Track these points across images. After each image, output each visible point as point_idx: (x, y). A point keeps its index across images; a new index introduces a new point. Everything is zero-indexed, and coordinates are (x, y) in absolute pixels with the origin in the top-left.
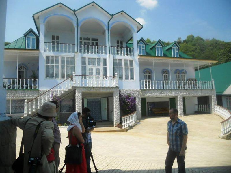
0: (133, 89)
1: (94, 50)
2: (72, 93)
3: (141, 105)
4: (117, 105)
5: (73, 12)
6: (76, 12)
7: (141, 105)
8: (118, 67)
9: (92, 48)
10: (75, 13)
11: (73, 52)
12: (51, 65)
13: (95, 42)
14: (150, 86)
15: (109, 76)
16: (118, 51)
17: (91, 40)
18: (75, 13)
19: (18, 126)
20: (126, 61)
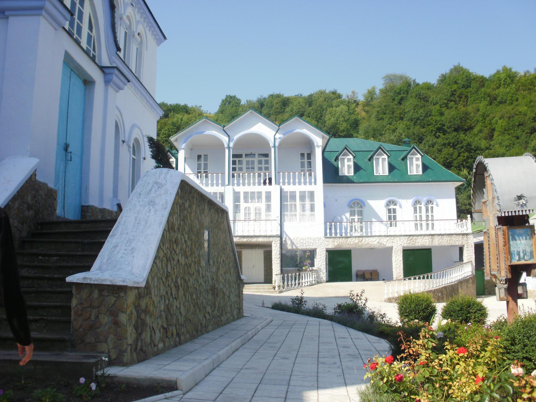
6: (225, 128)
8: (289, 203)
11: (223, 184)
14: (338, 231)
18: (224, 130)
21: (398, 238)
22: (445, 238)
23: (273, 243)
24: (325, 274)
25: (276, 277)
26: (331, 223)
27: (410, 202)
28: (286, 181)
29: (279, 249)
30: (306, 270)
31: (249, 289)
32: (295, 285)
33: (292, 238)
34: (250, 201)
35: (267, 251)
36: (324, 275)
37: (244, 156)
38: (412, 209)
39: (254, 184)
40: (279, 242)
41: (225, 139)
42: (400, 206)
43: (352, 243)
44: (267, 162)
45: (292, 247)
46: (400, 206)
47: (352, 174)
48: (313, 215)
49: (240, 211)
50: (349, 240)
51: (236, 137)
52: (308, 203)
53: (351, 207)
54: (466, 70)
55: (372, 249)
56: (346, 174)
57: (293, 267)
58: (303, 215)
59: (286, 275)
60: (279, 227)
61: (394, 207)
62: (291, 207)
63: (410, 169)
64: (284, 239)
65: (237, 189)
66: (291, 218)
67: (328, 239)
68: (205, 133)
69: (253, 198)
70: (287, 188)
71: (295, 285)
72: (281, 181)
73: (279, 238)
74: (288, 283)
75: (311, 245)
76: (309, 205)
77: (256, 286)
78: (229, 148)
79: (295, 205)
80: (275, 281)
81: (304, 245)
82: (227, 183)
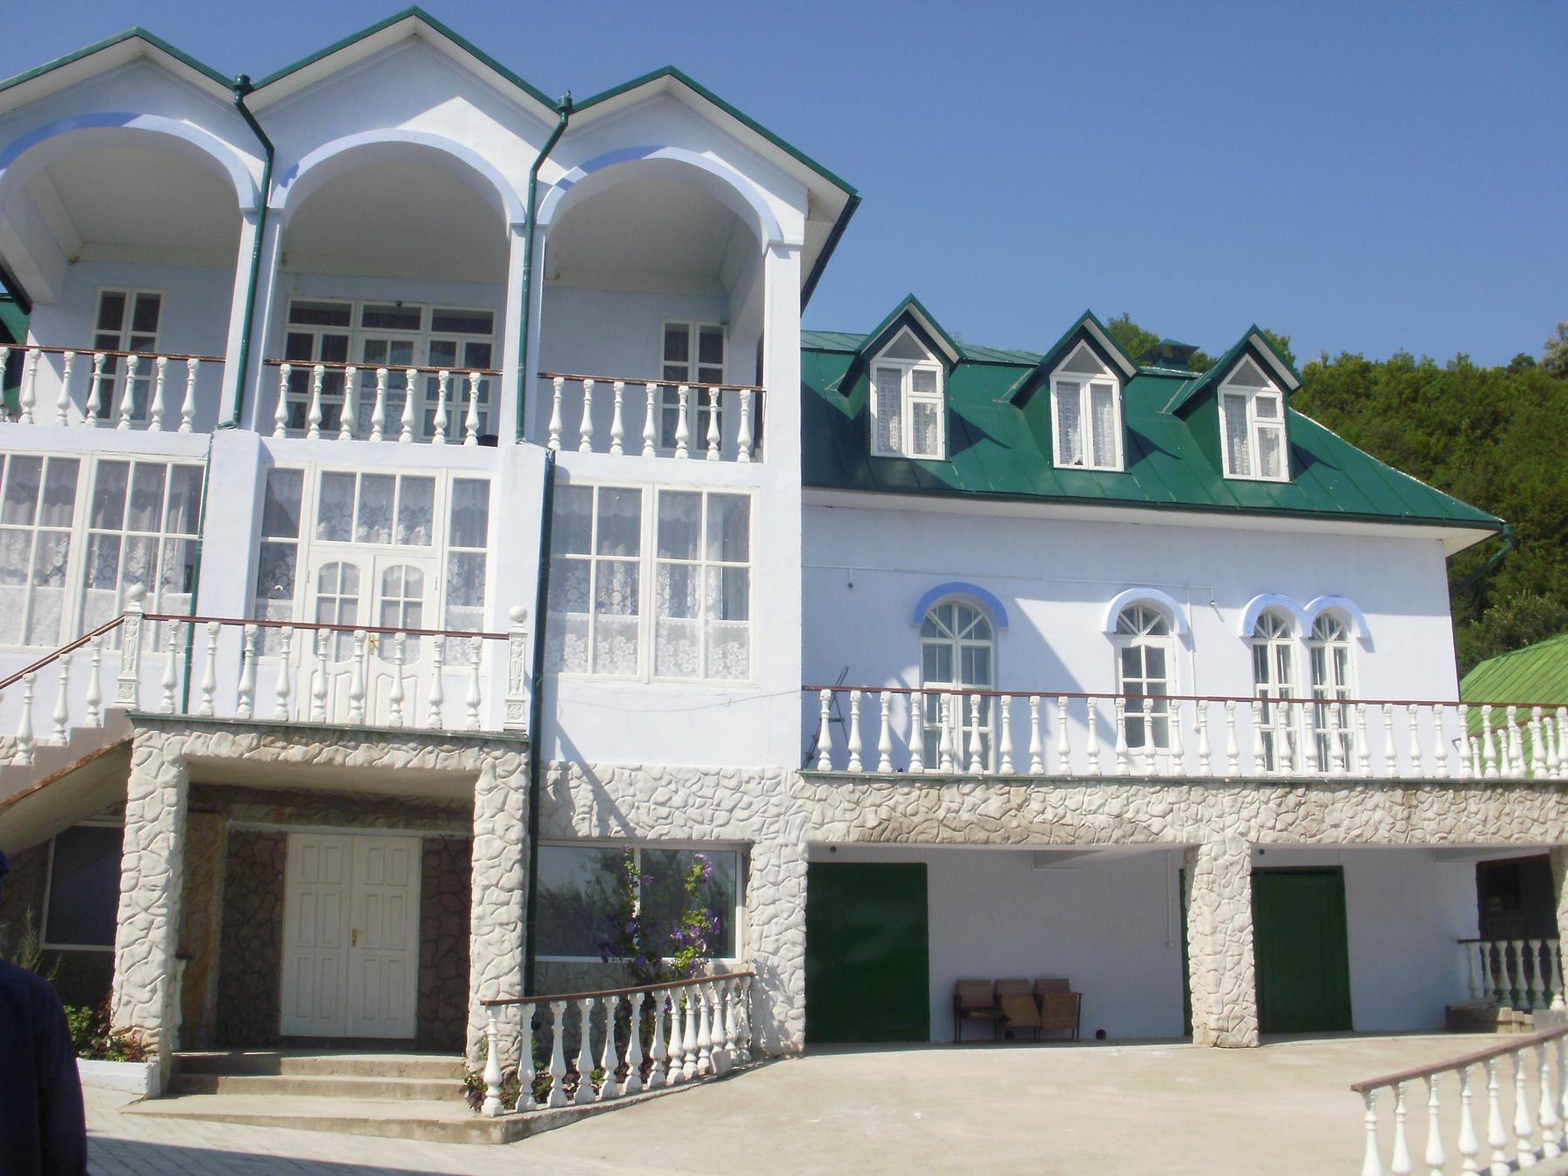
0: (729, 768)
1: (448, 413)
2: (104, 764)
3: (800, 915)
4: (504, 896)
5: (231, 97)
6: (250, 101)
7: (809, 921)
8: (593, 557)
9: (432, 393)
13: (462, 340)
15: (448, 634)
16: (668, 421)
17: (426, 319)
18: (241, 107)
20: (679, 505)
21: (1225, 799)
22: (1476, 803)
23: (481, 784)
24: (800, 1000)
25: (494, 1029)
26: (839, 690)
27: (1238, 619)
28: (586, 425)
29: (518, 830)
30: (683, 976)
31: (304, 1088)
32: (620, 1074)
33: (601, 773)
34: (356, 530)
35: (446, 843)
36: (789, 1013)
37: (357, 315)
38: (1248, 654)
39: (391, 429)
40: (519, 780)
41: (245, 167)
42: (1187, 639)
43: (965, 816)
44: (482, 357)
45: (603, 822)
46: (1187, 639)
47: (940, 455)
48: (740, 637)
49: (289, 585)
50: (950, 795)
51: (307, 163)
52: (706, 563)
53: (929, 629)
54: (1146, 334)
55: (1042, 858)
56: (909, 452)
57: (604, 949)
58: (677, 634)
59: (559, 1009)
60: (527, 696)
61: (1156, 642)
62: (605, 589)
63: (1231, 452)
64: (552, 776)
65: (287, 451)
66: (604, 647)
67: (822, 790)
68: (132, 124)
69: (374, 518)
70: (588, 468)
71: (620, 1074)
72: (555, 422)
73: (524, 758)
74: (570, 1068)
75: (721, 816)
76: (714, 581)
77: (357, 1069)
78: (262, 214)
79: (632, 569)
80: (483, 1046)
81: (678, 817)
82: (227, 411)
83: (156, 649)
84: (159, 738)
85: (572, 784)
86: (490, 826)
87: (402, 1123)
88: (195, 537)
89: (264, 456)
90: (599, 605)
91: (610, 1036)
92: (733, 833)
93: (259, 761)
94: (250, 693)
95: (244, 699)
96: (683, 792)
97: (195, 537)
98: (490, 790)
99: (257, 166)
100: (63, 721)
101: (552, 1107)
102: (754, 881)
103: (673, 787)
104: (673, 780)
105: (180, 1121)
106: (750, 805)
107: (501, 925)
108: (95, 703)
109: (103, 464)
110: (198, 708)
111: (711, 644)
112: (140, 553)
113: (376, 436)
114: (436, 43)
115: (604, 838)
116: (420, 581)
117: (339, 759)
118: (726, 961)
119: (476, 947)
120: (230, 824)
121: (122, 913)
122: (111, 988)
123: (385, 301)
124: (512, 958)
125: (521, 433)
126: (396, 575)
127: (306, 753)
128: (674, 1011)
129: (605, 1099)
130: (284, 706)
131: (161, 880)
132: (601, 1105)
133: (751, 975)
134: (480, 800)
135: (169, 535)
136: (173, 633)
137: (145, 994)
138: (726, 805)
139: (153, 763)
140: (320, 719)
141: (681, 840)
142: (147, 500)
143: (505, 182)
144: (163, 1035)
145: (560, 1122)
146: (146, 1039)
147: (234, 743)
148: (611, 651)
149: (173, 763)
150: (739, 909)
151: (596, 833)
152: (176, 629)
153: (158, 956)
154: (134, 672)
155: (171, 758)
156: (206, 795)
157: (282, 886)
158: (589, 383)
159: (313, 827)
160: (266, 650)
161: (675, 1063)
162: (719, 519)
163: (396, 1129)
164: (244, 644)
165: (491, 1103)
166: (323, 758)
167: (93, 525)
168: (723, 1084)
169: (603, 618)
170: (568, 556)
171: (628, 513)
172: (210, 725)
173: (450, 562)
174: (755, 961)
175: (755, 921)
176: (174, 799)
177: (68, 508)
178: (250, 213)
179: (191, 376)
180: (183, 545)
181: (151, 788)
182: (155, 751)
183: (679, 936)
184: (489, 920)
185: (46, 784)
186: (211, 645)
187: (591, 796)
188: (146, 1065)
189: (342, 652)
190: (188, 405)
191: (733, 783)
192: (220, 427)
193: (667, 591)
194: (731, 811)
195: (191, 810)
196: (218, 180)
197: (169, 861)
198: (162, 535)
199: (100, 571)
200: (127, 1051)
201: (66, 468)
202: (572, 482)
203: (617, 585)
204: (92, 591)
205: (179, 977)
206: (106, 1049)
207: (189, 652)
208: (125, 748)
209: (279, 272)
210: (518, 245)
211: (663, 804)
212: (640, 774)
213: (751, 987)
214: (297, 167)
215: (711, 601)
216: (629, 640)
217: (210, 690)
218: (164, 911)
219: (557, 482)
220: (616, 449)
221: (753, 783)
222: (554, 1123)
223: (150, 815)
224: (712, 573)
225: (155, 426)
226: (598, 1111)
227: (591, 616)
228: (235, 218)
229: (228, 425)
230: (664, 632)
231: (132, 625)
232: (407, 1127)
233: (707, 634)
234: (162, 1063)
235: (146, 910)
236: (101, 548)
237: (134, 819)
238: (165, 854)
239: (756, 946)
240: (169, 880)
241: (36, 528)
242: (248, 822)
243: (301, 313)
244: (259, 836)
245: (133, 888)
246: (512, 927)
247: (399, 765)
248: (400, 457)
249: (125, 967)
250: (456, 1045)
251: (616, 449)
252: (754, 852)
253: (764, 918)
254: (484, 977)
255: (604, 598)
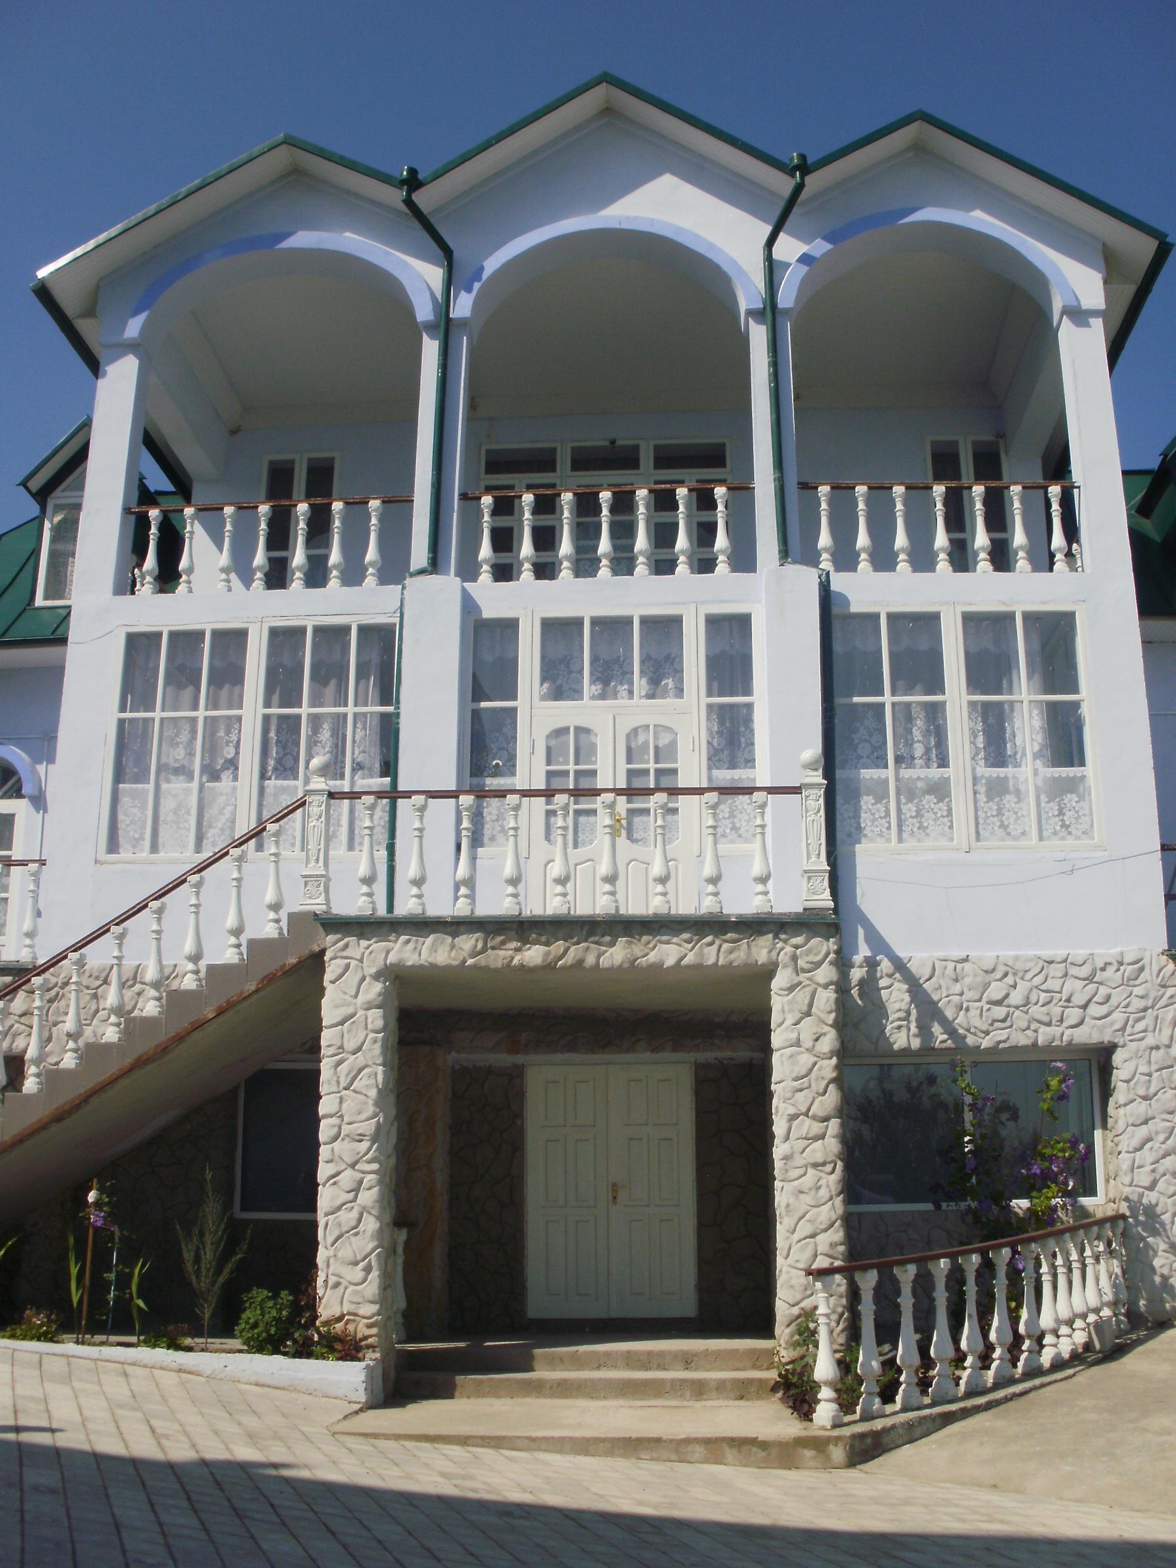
0: (1079, 953)
2: (289, 981)
4: (817, 1128)
5: (396, 197)
6: (419, 197)
8: (887, 699)
10: (409, 203)
12: (894, 705)
15: (772, 790)
17: (647, 457)
19: (409, 1233)
20: (986, 628)
30: (1042, 1224)
34: (588, 687)
37: (564, 460)
41: (421, 277)
45: (924, 1030)
51: (492, 264)
52: (1026, 702)
57: (937, 1193)
58: (997, 789)
64: (857, 974)
66: (909, 809)
69: (610, 674)
70: (869, 591)
72: (825, 539)
75: (1073, 1015)
78: (445, 327)
79: (935, 713)
82: (419, 554)
83: (351, 848)
84: (357, 947)
85: (883, 983)
86: (794, 1036)
87: (708, 1442)
88: (390, 709)
89: (469, 605)
90: (899, 760)
91: (971, 1308)
92: (1088, 1034)
93: (486, 969)
94: (470, 882)
95: (463, 890)
96: (1023, 987)
97: (390, 709)
98: (791, 989)
99: (434, 275)
100: (237, 932)
101: (904, 1409)
102: (1120, 1094)
103: (1010, 980)
104: (1011, 972)
105: (409, 1444)
106: (1108, 998)
107: (815, 1165)
108: (276, 907)
109: (274, 633)
110: (406, 906)
111: (1043, 798)
112: (325, 734)
113: (604, 572)
114: (637, 114)
115: (927, 1050)
116: (673, 745)
117: (590, 960)
118: (1085, 1201)
119: (782, 1196)
120: (451, 1059)
121: (324, 1171)
122: (316, 1266)
123: (596, 439)
124: (831, 1209)
125: (785, 554)
126: (641, 738)
127: (547, 954)
128: (1044, 1269)
129: (969, 1394)
130: (515, 896)
131: (369, 1127)
132: (969, 1403)
133: (1123, 1217)
134: (777, 1003)
135: (358, 708)
136: (370, 816)
137: (357, 1273)
138: (1079, 999)
139: (352, 978)
140: (563, 910)
141: (1025, 1047)
142: (329, 673)
143: (735, 263)
144: (383, 1326)
145: (918, 1431)
146: (362, 1331)
147: (453, 947)
148: (918, 814)
149: (377, 977)
150: (1098, 1134)
151: (916, 1044)
152: (372, 808)
153: (371, 1224)
154: (319, 866)
155: (373, 970)
156: (422, 1021)
157: (521, 1131)
158: (861, 490)
159: (559, 1057)
160: (486, 840)
161: (1048, 1339)
162: (1036, 646)
163: (699, 1450)
164: (459, 821)
165: (825, 1411)
166: (569, 959)
167: (267, 704)
168: (1113, 1366)
169: (905, 773)
170: (856, 699)
171: (924, 645)
172: (421, 925)
173: (708, 719)
174: (1127, 1199)
175: (1123, 1147)
176: (380, 1023)
177: (237, 688)
178: (431, 328)
179: (374, 521)
180: (376, 721)
181: (351, 1010)
182: (353, 963)
183: (1036, 1170)
184: (799, 1160)
185: (221, 1012)
186: (417, 825)
187: (907, 998)
188: (363, 1364)
189: (581, 837)
190: (372, 554)
191: (1084, 971)
192: (412, 575)
193: (980, 739)
194: (1085, 1007)
195: (402, 1042)
196: (388, 294)
197: (377, 1104)
198: (350, 709)
199: (279, 761)
200: (338, 1346)
201: (231, 642)
202: (854, 609)
203: (917, 734)
204: (270, 784)
205: (400, 1250)
206: (314, 1342)
207: (391, 849)
208: (316, 961)
209: (469, 420)
210: (758, 336)
211: (998, 1003)
212: (967, 965)
213: (1124, 1234)
214: (482, 269)
215: (1037, 748)
216: (940, 800)
217: (419, 882)
218: (375, 1166)
219: (835, 610)
220: (903, 566)
221: (1111, 970)
222: (913, 1433)
223: (350, 1045)
224: (1035, 712)
225: (334, 583)
226: (965, 1413)
227: (890, 773)
228: (412, 334)
229: (422, 572)
230: (982, 789)
231: (317, 806)
232: (717, 1448)
233: (1037, 788)
234: (383, 1360)
235: (353, 1166)
236: (278, 732)
237: (332, 1051)
238: (373, 1093)
239: (1127, 1180)
240: (379, 1127)
241: (201, 713)
242: (473, 1050)
243: (498, 463)
244: (490, 1071)
245: (335, 1139)
246: (829, 1168)
247: (670, 962)
248: (637, 595)
249: (330, 1240)
250: (763, 1325)
251: (903, 566)
252: (1118, 1058)
253: (1135, 1143)
254: (796, 1236)
255: (903, 750)
